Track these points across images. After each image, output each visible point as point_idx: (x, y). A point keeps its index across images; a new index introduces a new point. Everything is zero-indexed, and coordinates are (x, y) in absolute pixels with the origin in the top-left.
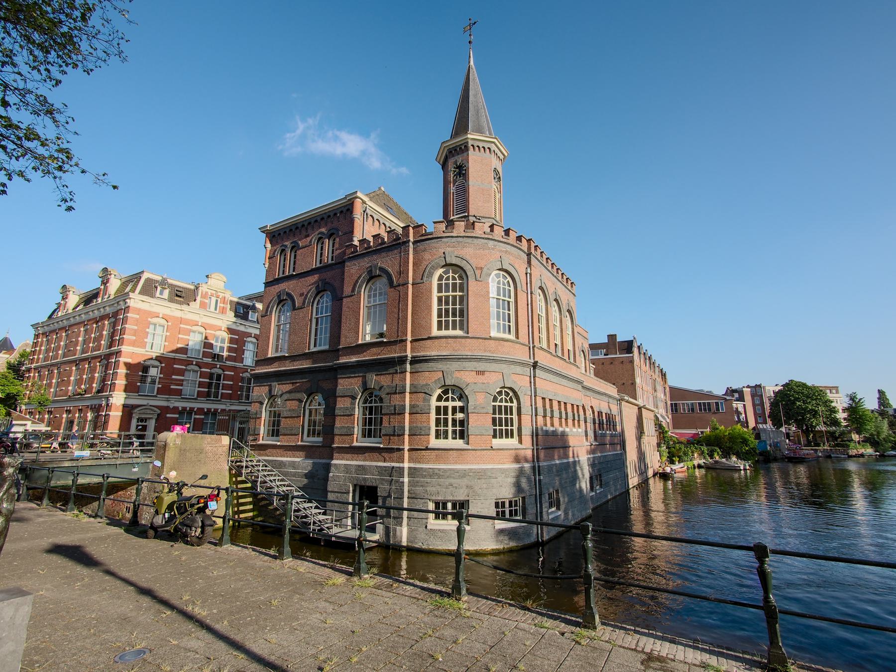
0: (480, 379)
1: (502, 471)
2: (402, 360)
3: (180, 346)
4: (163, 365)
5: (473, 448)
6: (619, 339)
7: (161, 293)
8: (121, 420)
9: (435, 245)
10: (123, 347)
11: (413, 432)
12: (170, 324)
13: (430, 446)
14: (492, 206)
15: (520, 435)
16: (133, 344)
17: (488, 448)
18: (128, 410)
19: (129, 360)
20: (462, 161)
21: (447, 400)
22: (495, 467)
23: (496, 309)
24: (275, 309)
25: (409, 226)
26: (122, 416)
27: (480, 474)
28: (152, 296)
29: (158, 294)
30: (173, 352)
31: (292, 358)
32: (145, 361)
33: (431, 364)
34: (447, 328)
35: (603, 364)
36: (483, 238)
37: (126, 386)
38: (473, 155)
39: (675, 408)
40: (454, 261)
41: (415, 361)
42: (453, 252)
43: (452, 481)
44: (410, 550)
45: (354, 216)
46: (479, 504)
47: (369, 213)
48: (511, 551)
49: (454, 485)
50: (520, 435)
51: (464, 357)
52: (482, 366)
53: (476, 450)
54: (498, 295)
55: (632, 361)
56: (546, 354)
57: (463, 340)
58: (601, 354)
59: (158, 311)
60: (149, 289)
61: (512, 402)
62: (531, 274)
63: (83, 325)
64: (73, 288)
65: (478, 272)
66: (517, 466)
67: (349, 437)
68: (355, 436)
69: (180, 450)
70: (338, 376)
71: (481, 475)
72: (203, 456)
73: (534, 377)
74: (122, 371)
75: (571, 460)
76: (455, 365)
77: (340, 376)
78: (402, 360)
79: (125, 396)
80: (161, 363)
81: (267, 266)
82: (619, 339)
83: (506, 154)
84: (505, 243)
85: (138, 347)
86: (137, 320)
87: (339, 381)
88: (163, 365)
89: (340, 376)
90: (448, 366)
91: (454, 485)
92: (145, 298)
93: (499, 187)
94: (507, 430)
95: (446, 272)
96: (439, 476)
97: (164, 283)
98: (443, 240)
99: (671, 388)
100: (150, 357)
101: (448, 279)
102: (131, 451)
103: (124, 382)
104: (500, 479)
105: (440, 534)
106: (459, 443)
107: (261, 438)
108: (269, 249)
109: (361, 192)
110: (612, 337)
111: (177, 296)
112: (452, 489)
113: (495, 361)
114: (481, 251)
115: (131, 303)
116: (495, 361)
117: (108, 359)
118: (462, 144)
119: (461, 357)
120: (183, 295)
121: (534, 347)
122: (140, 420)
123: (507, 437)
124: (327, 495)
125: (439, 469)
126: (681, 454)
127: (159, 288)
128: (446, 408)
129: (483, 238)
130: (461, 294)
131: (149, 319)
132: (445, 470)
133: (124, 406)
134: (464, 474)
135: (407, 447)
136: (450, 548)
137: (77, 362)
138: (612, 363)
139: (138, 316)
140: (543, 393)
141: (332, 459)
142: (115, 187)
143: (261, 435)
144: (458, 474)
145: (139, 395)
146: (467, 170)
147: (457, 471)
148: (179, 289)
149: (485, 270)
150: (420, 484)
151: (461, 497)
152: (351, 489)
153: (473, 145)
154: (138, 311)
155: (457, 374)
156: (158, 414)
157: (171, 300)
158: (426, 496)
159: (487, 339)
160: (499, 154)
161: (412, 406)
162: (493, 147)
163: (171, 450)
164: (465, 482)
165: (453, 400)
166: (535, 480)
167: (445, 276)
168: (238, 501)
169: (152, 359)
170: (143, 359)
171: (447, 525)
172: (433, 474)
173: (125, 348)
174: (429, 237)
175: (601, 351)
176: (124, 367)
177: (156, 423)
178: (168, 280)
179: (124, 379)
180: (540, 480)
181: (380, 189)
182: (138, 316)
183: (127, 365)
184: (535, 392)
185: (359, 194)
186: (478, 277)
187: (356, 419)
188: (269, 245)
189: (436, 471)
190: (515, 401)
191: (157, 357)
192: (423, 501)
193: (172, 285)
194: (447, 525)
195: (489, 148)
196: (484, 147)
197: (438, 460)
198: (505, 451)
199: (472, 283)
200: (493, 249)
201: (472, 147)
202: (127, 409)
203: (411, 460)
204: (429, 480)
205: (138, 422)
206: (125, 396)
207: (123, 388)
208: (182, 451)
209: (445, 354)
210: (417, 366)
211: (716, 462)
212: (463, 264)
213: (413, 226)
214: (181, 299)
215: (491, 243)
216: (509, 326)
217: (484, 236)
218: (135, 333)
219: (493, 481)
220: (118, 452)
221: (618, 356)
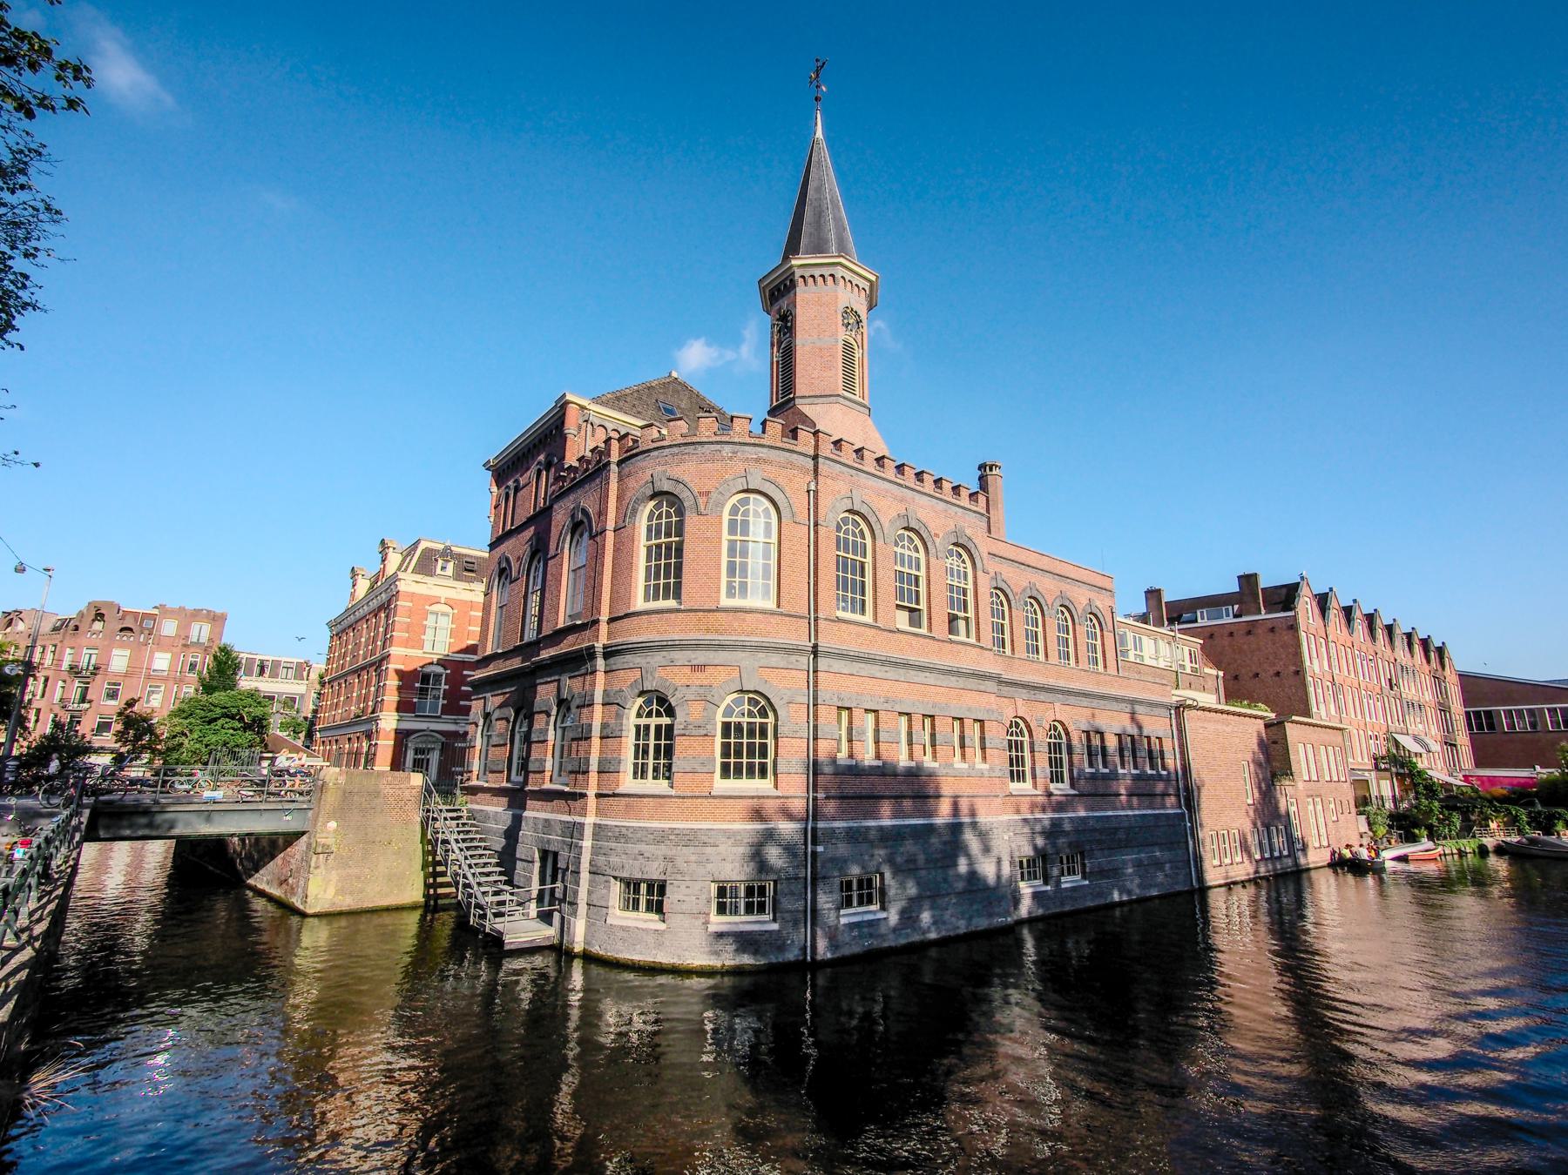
0: (700, 678)
1: (728, 834)
2: (590, 654)
3: (471, 642)
4: (449, 671)
5: (679, 793)
6: (1264, 583)
7: (443, 568)
8: (394, 751)
9: (640, 464)
10: (393, 648)
11: (602, 769)
12: (456, 611)
13: (620, 790)
14: (836, 375)
15: (1034, 777)
16: (406, 643)
17: (704, 794)
18: (402, 736)
19: (402, 667)
20: (788, 305)
21: (649, 715)
22: (715, 827)
23: (761, 561)
24: (496, 583)
25: (610, 438)
26: (395, 746)
27: (688, 837)
28: (431, 573)
29: (439, 571)
30: (458, 652)
31: (506, 655)
32: (422, 667)
33: (628, 657)
34: (656, 598)
35: (1231, 634)
36: (712, 443)
37: (399, 702)
38: (803, 293)
39: (1481, 724)
40: (666, 486)
41: (609, 653)
42: (665, 472)
43: (643, 847)
44: (589, 958)
45: (566, 431)
46: (683, 887)
47: (597, 422)
48: (737, 972)
49: (646, 855)
50: (1034, 777)
51: (670, 643)
52: (700, 657)
53: (684, 797)
54: (766, 537)
55: (1293, 627)
56: (873, 631)
57: (673, 616)
58: (1228, 615)
59: (438, 594)
60: (426, 564)
61: (766, 716)
62: (816, 492)
63: (364, 621)
64: (363, 570)
65: (701, 500)
66: (759, 826)
67: (538, 776)
68: (548, 774)
69: (344, 792)
70: (538, 681)
71: (690, 839)
72: (377, 801)
73: (815, 671)
74: (392, 682)
75: (940, 820)
76: (658, 658)
77: (542, 681)
78: (590, 654)
79: (397, 718)
80: (446, 669)
81: (492, 519)
82: (1264, 583)
83: (873, 278)
84: (755, 445)
85: (413, 647)
86: (410, 609)
87: (539, 688)
88: (449, 671)
89: (542, 681)
90: (649, 659)
91: (646, 855)
92: (419, 577)
93: (859, 337)
94: (1018, 771)
95: (658, 506)
96: (627, 840)
97: (447, 554)
98: (652, 454)
99: (1465, 678)
100: (430, 661)
101: (660, 517)
102: (283, 793)
103: (396, 698)
104: (722, 848)
105: (621, 934)
106: (662, 786)
107: (475, 777)
108: (495, 494)
109: (571, 393)
110: (1248, 581)
111: (466, 570)
112: (643, 861)
113: (721, 647)
114: (710, 465)
115: (402, 586)
116: (721, 647)
117: (378, 665)
118: (786, 279)
119: (665, 643)
120: (476, 567)
121: (816, 619)
122: (417, 751)
123: (1019, 781)
124: (515, 863)
125: (627, 828)
126: (1434, 821)
127: (440, 562)
128: (647, 727)
129: (712, 443)
130: (677, 539)
131: (427, 607)
132: (635, 830)
133: (397, 732)
134: (661, 837)
135: (591, 792)
136: (634, 958)
137: (354, 672)
138: (1249, 633)
139: (411, 604)
140: (839, 699)
141: (525, 809)
142: (37, 465)
143: (475, 773)
144: (652, 837)
145: (417, 716)
146: (793, 321)
147: (652, 831)
148: (469, 560)
149: (714, 495)
150: (602, 851)
151: (655, 874)
152: (537, 856)
153: (803, 277)
154: (412, 596)
155: (660, 673)
156: (443, 743)
157: (457, 577)
158: (609, 871)
159: (713, 611)
160: (856, 280)
161: (604, 726)
162: (839, 272)
163: (329, 793)
164: (662, 850)
165: (659, 714)
166: (806, 853)
167: (742, 509)
168: (434, 869)
169: (432, 663)
170: (421, 664)
171: (636, 919)
172: (621, 836)
173: (395, 650)
174: (634, 452)
175: (1227, 610)
176: (396, 677)
177: (441, 756)
178: (453, 548)
179: (396, 693)
180: (814, 853)
181: (670, 376)
182: (411, 604)
183: (398, 672)
184: (816, 698)
185: (569, 397)
186: (702, 507)
187: (550, 748)
188: (495, 489)
189: (624, 831)
190: (771, 714)
191: (439, 660)
192: (605, 878)
193: (460, 554)
194: (636, 919)
195: (832, 275)
196: (822, 276)
197: (628, 812)
198: (738, 800)
199: (691, 520)
200: (731, 458)
201: (801, 280)
202: (400, 736)
203: (599, 812)
204: (613, 845)
205: (416, 754)
206: (397, 718)
207: (395, 705)
208: (346, 795)
209: (640, 640)
210: (612, 660)
211: (1532, 841)
212: (678, 490)
213: (617, 436)
214: (473, 575)
215: (727, 448)
216: (863, 583)
217: (748, 440)
218: (408, 628)
219: (709, 850)
220: (263, 793)
221: (1263, 616)
